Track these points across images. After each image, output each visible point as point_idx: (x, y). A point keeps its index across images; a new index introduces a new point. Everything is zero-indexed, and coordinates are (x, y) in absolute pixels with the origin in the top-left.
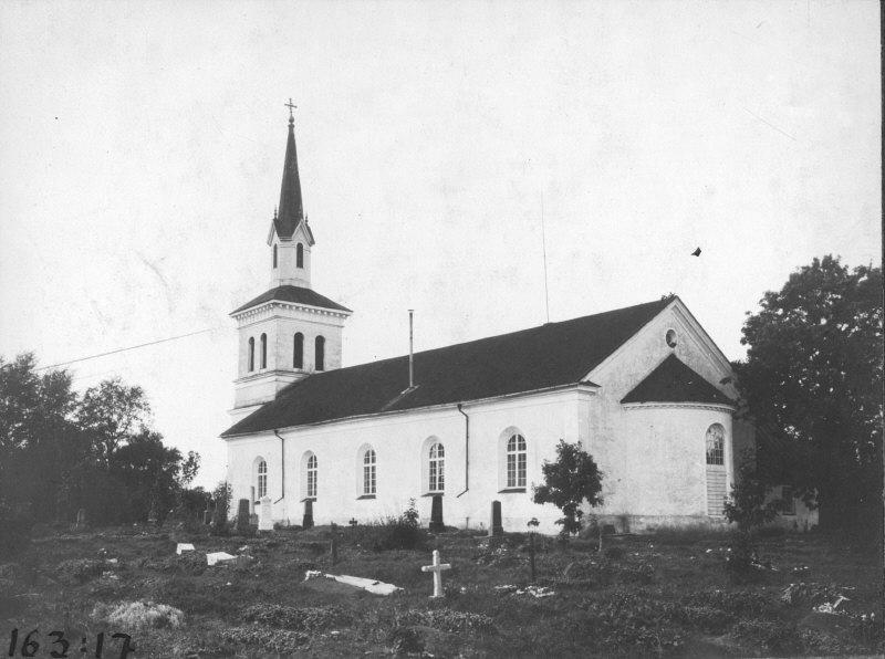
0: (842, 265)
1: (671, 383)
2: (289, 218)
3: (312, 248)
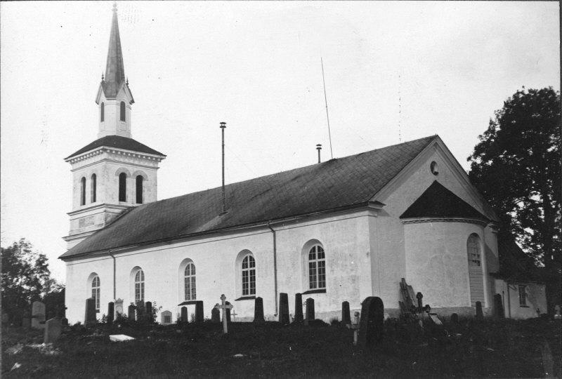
0: (29, 259)
1: (434, 205)
2: (115, 82)
3: (133, 106)
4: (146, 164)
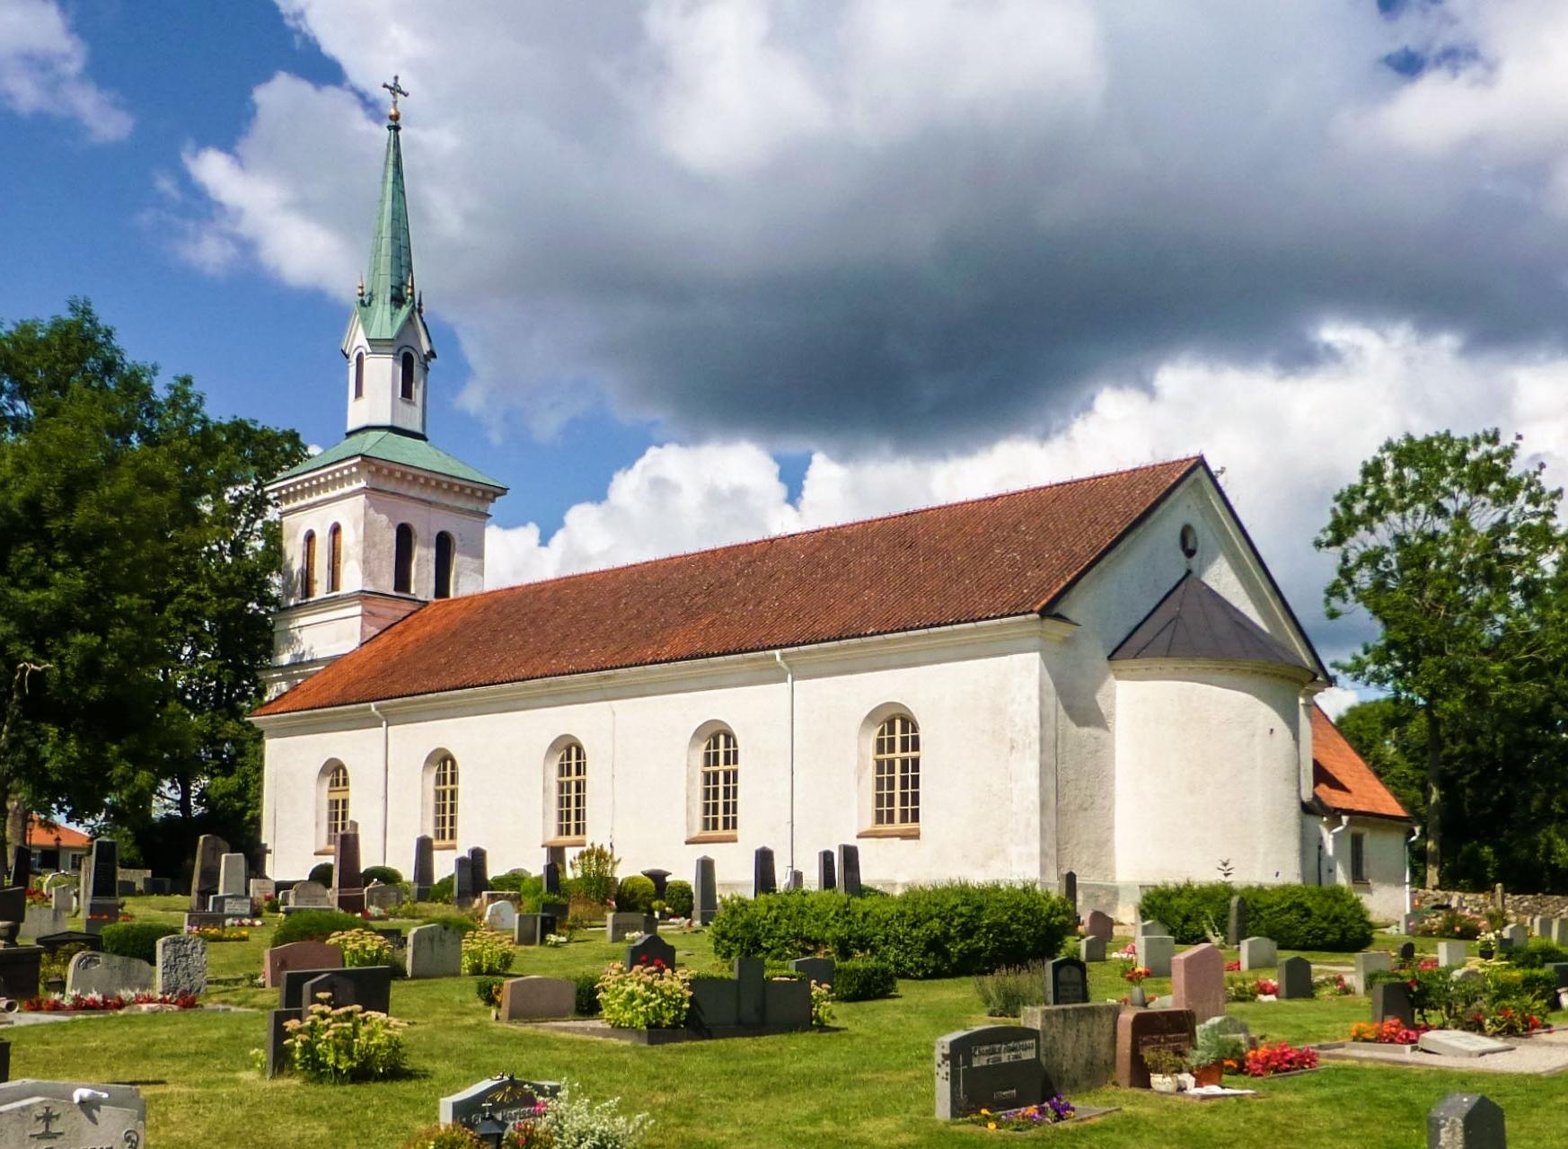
4: (459, 504)
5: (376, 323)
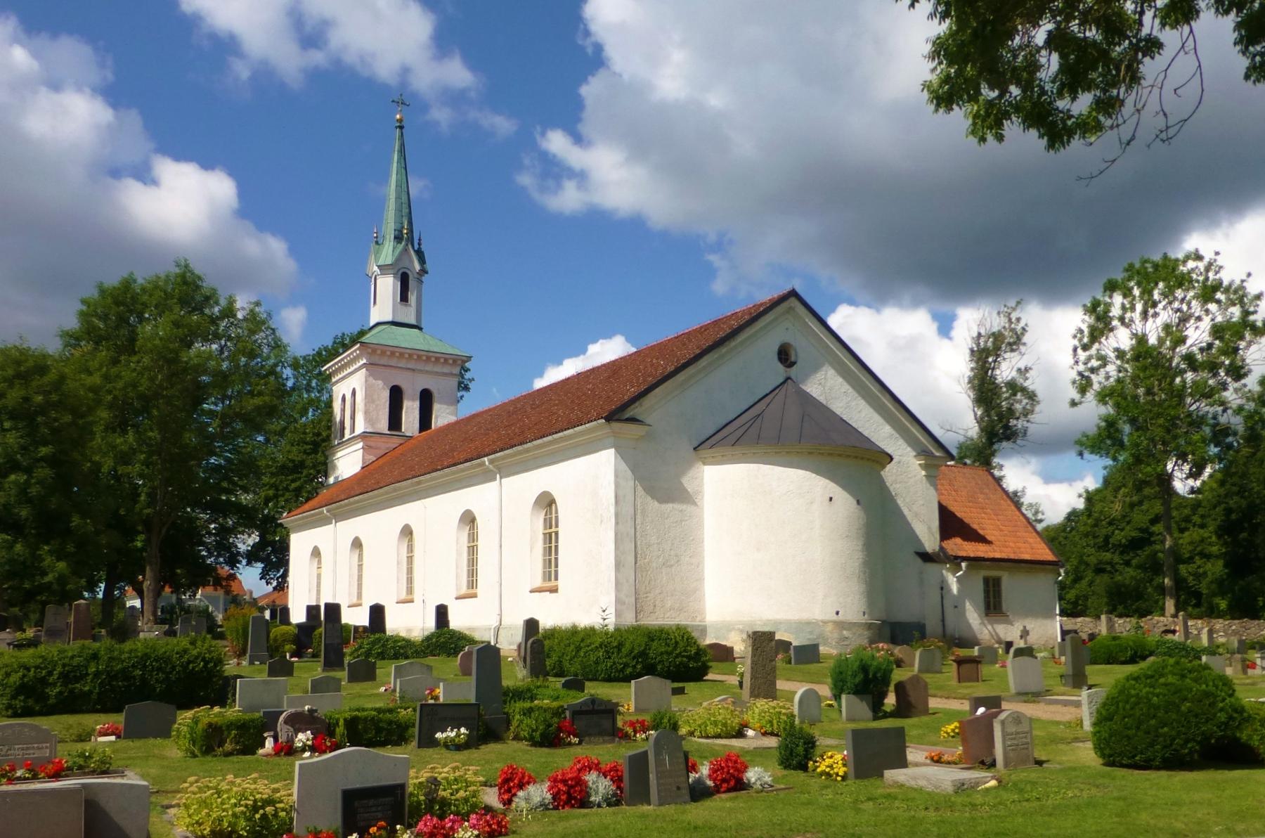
5: (383, 256)
